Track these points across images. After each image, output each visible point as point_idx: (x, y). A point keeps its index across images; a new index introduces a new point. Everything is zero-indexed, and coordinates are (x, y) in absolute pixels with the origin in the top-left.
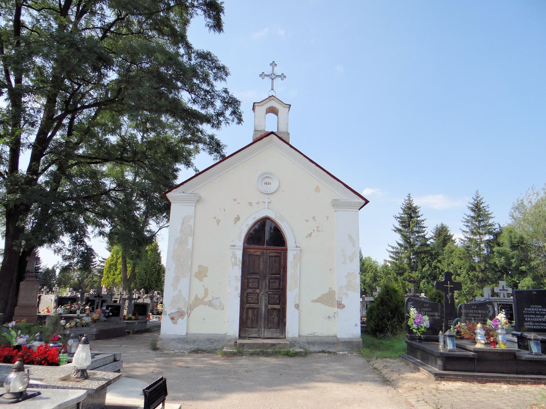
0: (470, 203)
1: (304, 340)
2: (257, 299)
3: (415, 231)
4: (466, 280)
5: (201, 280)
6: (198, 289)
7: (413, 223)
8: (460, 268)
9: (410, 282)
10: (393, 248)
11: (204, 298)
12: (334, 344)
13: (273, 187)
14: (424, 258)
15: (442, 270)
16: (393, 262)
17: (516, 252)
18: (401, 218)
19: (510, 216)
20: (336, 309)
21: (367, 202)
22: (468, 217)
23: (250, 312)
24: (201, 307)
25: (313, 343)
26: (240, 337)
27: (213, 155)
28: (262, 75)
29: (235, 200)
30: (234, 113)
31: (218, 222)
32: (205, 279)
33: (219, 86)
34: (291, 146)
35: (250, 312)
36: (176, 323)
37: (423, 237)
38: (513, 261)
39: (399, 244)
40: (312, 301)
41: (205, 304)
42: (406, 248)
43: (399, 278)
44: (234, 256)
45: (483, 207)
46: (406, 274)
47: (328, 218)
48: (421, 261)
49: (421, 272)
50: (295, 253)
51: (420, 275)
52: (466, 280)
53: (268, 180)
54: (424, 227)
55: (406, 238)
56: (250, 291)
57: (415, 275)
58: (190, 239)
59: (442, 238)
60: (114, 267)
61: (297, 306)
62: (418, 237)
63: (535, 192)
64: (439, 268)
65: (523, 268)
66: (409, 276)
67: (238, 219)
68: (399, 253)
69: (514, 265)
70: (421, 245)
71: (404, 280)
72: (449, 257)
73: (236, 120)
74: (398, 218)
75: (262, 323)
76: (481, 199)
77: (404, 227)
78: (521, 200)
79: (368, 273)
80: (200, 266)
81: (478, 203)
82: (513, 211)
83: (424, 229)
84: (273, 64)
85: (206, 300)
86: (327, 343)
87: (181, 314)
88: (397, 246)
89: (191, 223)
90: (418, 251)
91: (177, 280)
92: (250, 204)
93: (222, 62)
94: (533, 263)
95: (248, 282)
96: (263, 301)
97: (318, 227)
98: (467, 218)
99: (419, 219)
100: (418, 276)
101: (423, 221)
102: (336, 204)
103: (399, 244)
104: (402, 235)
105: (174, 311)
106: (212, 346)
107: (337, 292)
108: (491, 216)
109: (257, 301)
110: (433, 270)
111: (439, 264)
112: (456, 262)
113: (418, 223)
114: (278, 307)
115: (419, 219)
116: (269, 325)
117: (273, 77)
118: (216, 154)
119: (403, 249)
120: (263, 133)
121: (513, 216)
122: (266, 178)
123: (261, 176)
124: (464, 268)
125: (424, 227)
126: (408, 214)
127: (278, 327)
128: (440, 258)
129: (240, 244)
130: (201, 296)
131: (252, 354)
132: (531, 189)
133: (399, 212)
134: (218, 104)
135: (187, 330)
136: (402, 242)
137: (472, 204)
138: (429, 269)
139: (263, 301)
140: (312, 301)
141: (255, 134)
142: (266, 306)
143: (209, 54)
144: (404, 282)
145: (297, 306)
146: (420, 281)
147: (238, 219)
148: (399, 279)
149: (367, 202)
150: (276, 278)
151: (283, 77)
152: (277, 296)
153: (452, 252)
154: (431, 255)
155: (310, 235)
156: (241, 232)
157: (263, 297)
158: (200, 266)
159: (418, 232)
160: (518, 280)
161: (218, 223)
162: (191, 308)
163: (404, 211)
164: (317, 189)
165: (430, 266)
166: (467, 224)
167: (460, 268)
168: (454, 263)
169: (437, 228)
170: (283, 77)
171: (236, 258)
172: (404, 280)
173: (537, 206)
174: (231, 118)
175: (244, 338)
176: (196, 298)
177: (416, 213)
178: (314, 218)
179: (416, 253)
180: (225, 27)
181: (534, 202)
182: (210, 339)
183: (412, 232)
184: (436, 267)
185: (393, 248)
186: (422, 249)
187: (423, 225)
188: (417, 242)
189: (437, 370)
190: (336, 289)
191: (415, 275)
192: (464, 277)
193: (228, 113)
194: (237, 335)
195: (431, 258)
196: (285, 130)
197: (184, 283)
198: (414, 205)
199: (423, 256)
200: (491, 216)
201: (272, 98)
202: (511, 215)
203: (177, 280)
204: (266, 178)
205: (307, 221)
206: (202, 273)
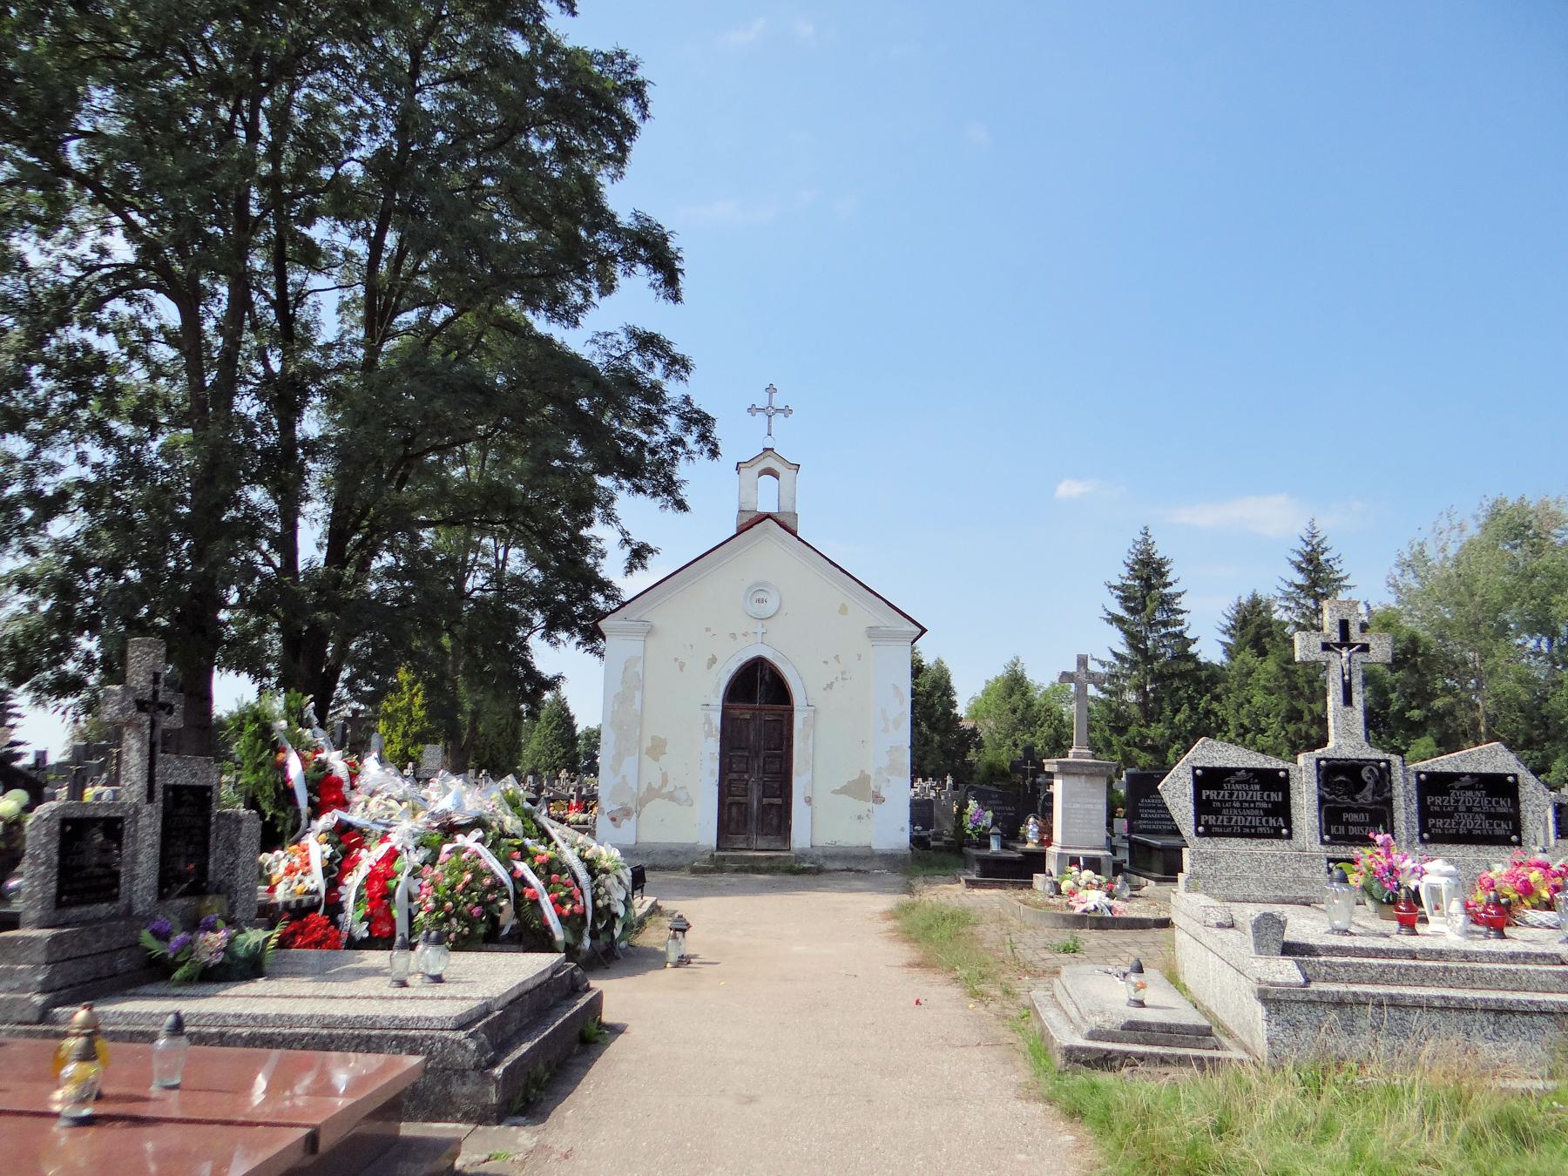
0: (1294, 551)
1: (819, 852)
2: (746, 790)
3: (1159, 622)
4: (1281, 744)
5: (656, 759)
6: (652, 775)
7: (1152, 601)
8: (1267, 716)
9: (1144, 749)
10: (1103, 664)
11: (661, 787)
12: (866, 857)
13: (771, 606)
14: (1178, 689)
15: (1223, 720)
16: (1102, 701)
17: (1400, 674)
18: (1123, 588)
19: (1390, 585)
20: (870, 805)
21: (924, 631)
22: (1290, 585)
23: (734, 810)
24: (657, 802)
25: (833, 857)
26: (719, 848)
27: (659, 499)
28: (753, 410)
29: (708, 630)
30: (703, 438)
31: (682, 666)
32: (663, 758)
33: (673, 390)
34: (799, 539)
35: (734, 810)
36: (619, 826)
37: (1180, 635)
38: (1393, 696)
39: (1115, 654)
40: (835, 792)
41: (664, 797)
42: (1134, 665)
43: (1115, 739)
44: (708, 721)
45: (1328, 561)
46: (1133, 730)
47: (860, 656)
48: (1171, 696)
49: (1171, 725)
50: (805, 715)
51: (1168, 733)
52: (1281, 744)
53: (761, 596)
54: (1182, 612)
55: (1134, 639)
56: (735, 776)
57: (1157, 731)
58: (638, 694)
59: (1251, 630)
60: (405, 717)
61: (809, 801)
62: (1164, 636)
63: (1456, 522)
64: (1215, 714)
65: (1416, 714)
66: (1140, 734)
67: (713, 660)
68: (1118, 678)
69: (1395, 707)
70: (1173, 657)
71: (1128, 744)
72: (1241, 687)
73: (706, 454)
74: (1115, 588)
75: (753, 826)
76: (1322, 541)
77: (1132, 611)
78: (1419, 544)
79: (1041, 726)
80: (653, 738)
81: (1313, 550)
82: (1397, 572)
83: (1180, 617)
84: (771, 389)
85: (665, 790)
86: (854, 857)
87: (627, 813)
88: (1112, 659)
89: (639, 668)
90: (1165, 671)
91: (618, 759)
92: (733, 636)
93: (676, 350)
94: (1438, 704)
95: (731, 762)
96: (755, 792)
97: (843, 673)
98: (1287, 589)
99: (1167, 591)
100: (1162, 735)
101: (1179, 595)
102: (874, 634)
103: (1115, 654)
104: (1126, 632)
105: (615, 807)
106: (677, 862)
107: (873, 778)
108: (1346, 583)
109: (746, 792)
110: (1200, 719)
111: (1215, 705)
112: (1259, 699)
113: (1166, 602)
114: (778, 801)
115: (1167, 591)
116: (764, 831)
117: (770, 412)
118: (665, 496)
119: (1127, 666)
120: (753, 515)
121: (1396, 586)
122: (758, 592)
123: (750, 588)
124: (1277, 715)
125: (1182, 612)
126: (1141, 578)
127: (779, 833)
128: (1219, 689)
129: (717, 701)
130: (656, 785)
131: (736, 871)
132: (1445, 515)
133: (1118, 572)
134: (672, 421)
135: (637, 837)
136: (1124, 650)
137: (1299, 553)
138: (1190, 717)
139: (755, 792)
140: (835, 792)
141: (739, 518)
142: (760, 801)
143: (656, 336)
144: (1127, 749)
145: (809, 801)
146: (1169, 747)
147: (713, 660)
148: (1114, 742)
149: (924, 631)
150: (776, 756)
151: (787, 411)
152: (776, 785)
153: (1249, 674)
154: (1198, 681)
155: (830, 686)
156: (718, 684)
157: (755, 787)
158: (653, 738)
159: (1165, 624)
160: (1404, 743)
161: (681, 669)
162: (642, 803)
163: (1132, 569)
164: (843, 609)
165: (1194, 709)
166: (1287, 604)
167: (1267, 716)
168: (1254, 701)
169: (1240, 605)
170: (787, 411)
171: (711, 724)
172: (1128, 744)
173: (1458, 562)
174: (696, 448)
175: (725, 850)
176: (650, 788)
177: (1162, 575)
178: (837, 657)
179: (1158, 677)
180: (684, 295)
181: (1452, 551)
182: (671, 852)
183: (1151, 625)
184: (1208, 713)
185: (1103, 664)
186: (1175, 667)
187: (1179, 607)
188: (1162, 651)
189: (974, 877)
190: (870, 772)
191: (1157, 731)
192: (1276, 738)
193: (690, 440)
194: (715, 845)
195: (1195, 690)
196: (789, 509)
197: (629, 766)
198: (1157, 556)
199: (1176, 683)
200: (1346, 583)
201: (769, 453)
202: (1391, 581)
203: (618, 759)
204: (758, 592)
205: (826, 662)
206: (657, 749)
